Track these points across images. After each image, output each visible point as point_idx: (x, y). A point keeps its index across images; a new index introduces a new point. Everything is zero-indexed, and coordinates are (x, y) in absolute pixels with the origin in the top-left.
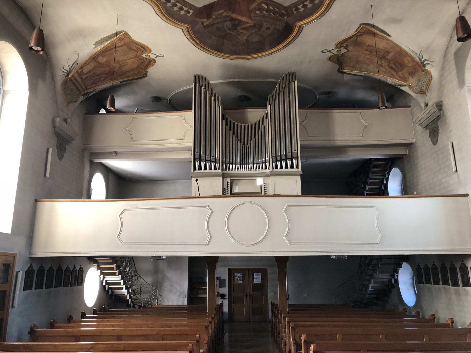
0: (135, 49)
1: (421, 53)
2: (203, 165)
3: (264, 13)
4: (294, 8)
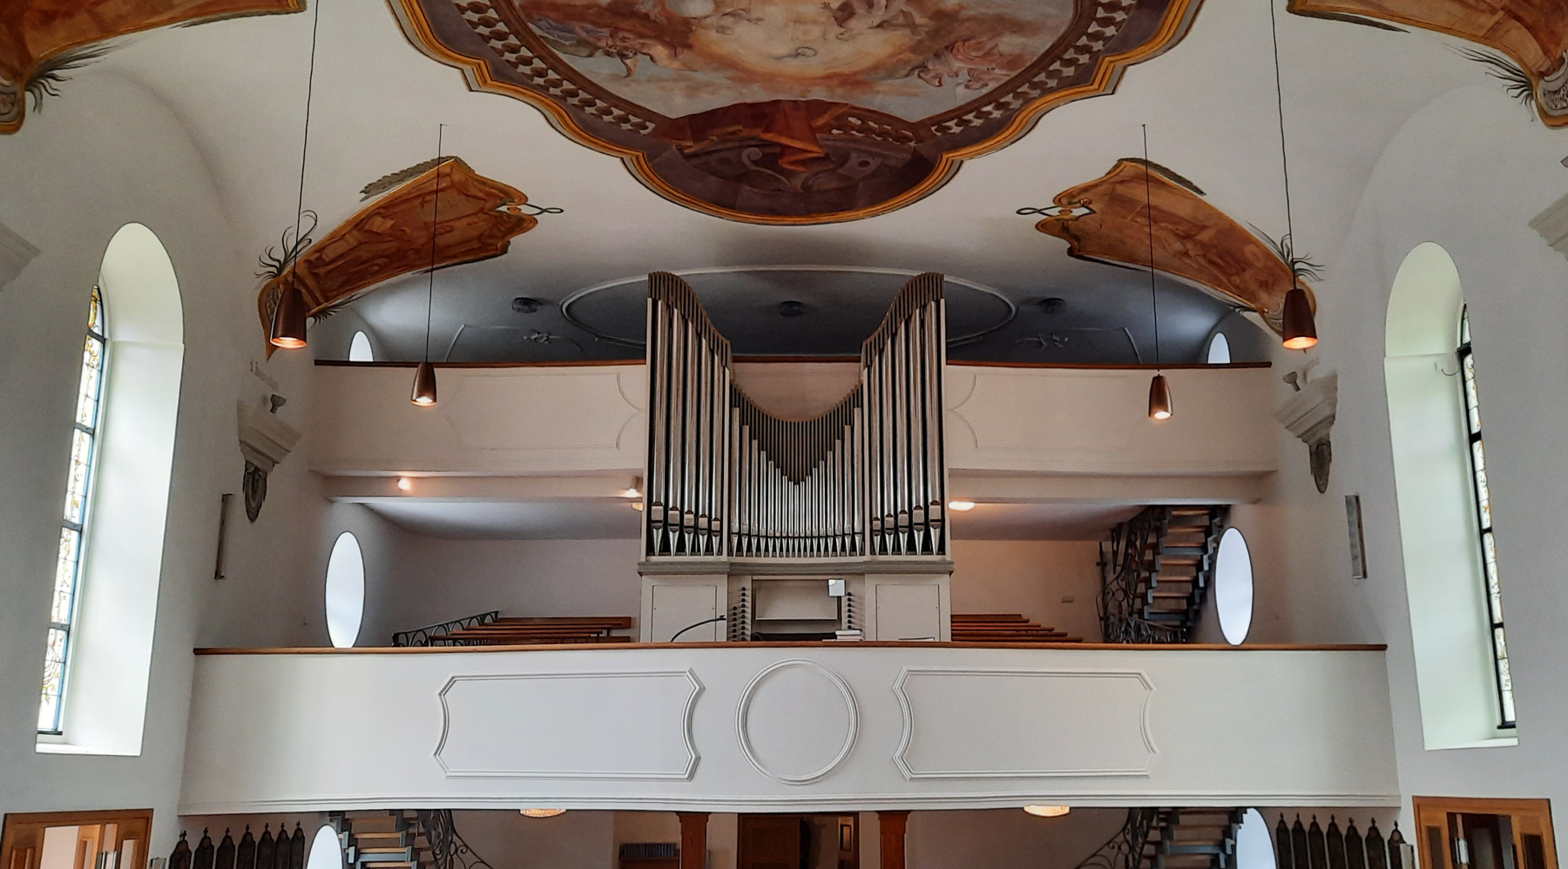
0: (481, 195)
1: (1284, 243)
2: (673, 538)
3: (853, 135)
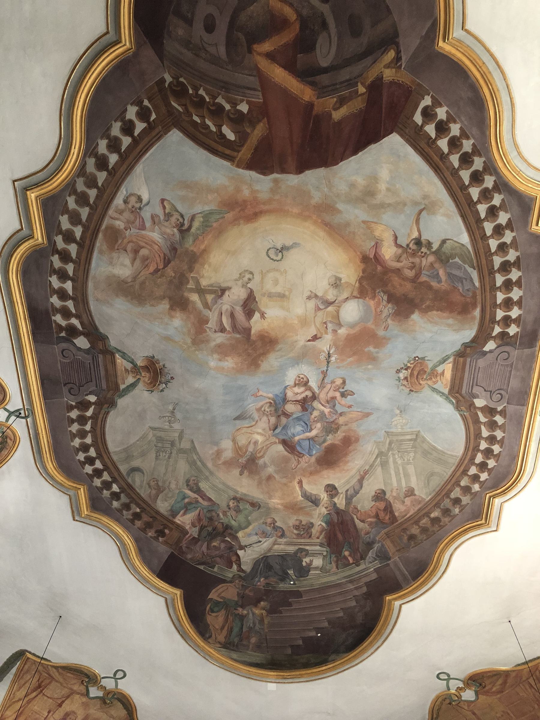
4: (153, 120)
